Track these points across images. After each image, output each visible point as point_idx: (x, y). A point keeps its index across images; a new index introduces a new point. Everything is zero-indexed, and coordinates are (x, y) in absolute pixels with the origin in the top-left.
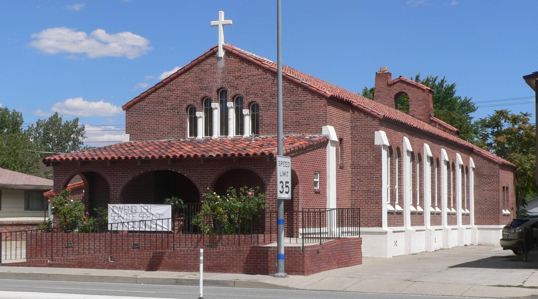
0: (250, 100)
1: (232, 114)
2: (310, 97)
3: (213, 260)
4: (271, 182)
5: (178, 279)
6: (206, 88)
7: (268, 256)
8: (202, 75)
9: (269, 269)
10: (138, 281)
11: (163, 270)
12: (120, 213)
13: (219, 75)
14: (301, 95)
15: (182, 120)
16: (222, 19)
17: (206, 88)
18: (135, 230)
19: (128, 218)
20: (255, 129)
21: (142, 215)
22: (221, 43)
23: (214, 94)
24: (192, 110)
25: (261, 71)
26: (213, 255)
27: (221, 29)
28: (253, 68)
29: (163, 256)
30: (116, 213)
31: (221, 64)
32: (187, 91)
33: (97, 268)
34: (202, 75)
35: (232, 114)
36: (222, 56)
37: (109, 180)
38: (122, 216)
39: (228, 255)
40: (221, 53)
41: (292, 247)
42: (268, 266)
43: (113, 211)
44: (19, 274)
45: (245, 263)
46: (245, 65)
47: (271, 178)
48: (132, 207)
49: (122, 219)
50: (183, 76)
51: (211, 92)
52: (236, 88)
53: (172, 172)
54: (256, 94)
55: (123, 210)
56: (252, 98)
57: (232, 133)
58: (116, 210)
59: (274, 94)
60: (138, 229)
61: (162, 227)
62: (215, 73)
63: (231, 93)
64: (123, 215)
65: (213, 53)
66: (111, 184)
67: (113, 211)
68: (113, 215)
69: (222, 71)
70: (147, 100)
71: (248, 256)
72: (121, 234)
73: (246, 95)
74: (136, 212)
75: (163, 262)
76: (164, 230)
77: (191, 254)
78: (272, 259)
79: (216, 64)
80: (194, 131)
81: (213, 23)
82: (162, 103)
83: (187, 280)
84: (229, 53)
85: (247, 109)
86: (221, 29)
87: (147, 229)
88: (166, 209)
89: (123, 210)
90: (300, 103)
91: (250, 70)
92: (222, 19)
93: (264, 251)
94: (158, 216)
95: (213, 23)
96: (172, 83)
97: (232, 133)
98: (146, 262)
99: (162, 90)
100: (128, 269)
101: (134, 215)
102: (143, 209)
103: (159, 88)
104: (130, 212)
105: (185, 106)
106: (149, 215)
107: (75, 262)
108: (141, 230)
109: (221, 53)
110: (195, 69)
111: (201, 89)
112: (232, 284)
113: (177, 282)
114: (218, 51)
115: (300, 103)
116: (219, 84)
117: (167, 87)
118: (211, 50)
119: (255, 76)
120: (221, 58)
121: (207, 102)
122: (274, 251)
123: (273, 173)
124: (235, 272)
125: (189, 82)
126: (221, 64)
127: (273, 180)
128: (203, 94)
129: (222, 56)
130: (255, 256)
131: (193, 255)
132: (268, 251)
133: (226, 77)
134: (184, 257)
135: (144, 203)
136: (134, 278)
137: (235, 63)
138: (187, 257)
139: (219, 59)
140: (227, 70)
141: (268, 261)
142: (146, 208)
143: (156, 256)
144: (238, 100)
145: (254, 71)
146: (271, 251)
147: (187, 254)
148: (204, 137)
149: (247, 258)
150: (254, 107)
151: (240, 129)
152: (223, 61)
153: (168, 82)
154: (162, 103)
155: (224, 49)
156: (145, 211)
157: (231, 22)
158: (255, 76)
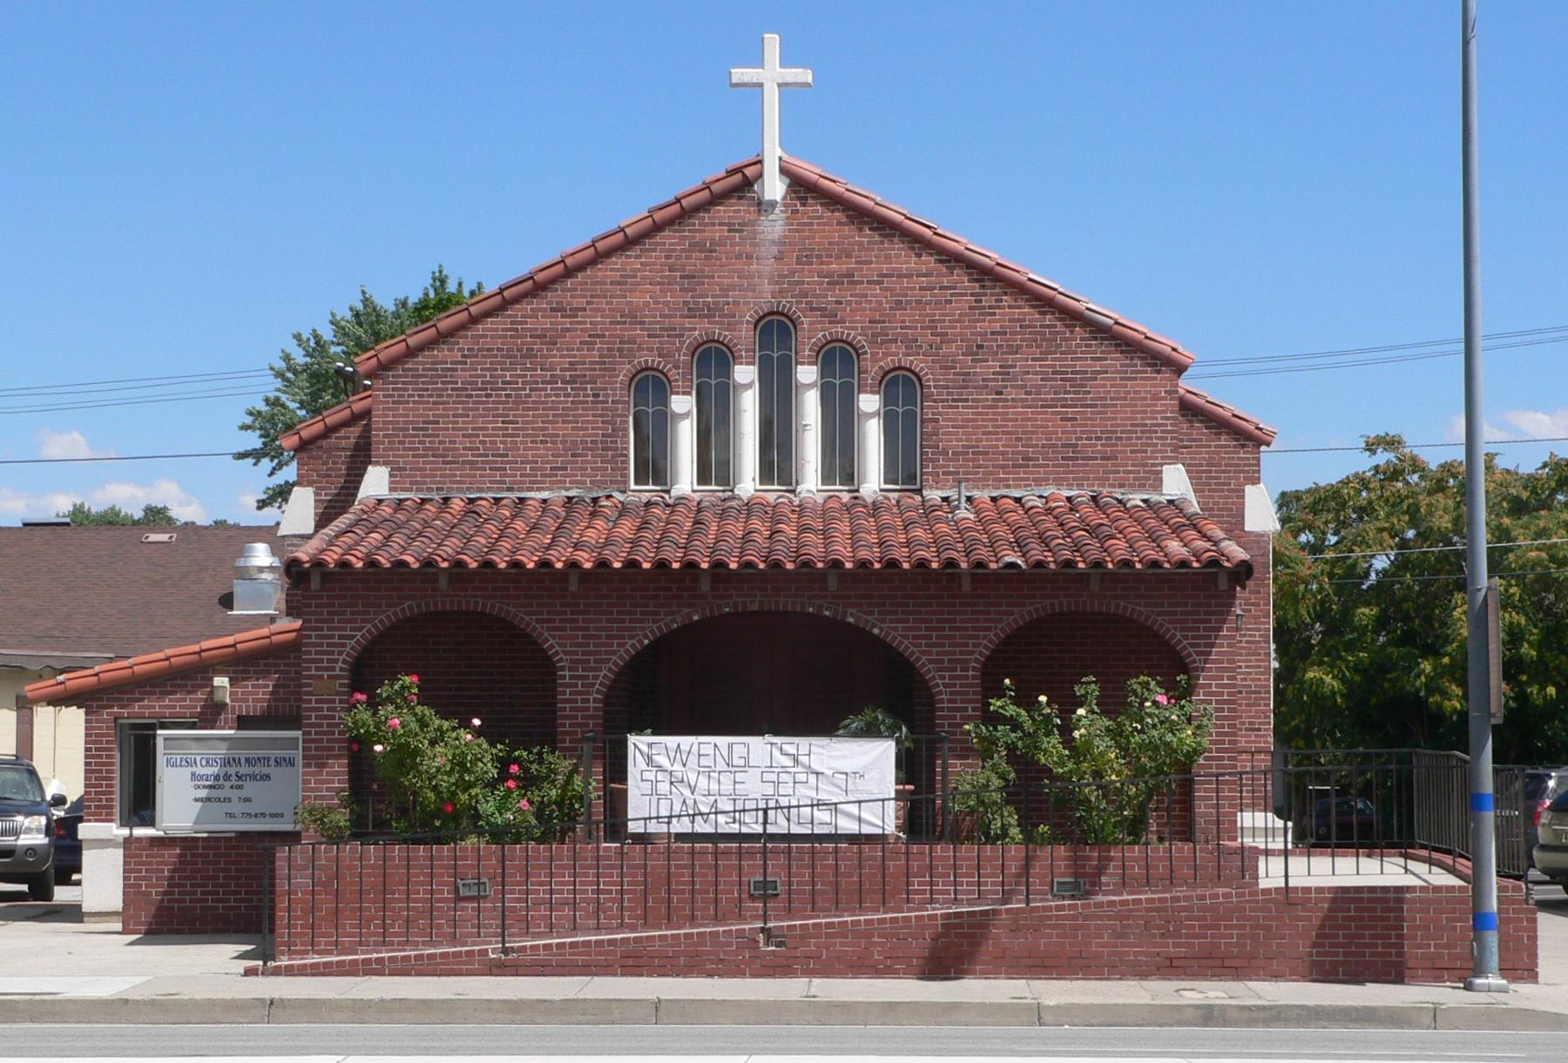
0: (889, 362)
1: (811, 407)
2: (1115, 361)
3: (1188, 936)
4: (1214, 662)
5: (1210, 1007)
6: (711, 312)
7: (1402, 919)
8: (695, 262)
9: (1410, 963)
10: (1046, 1018)
11: (985, 974)
12: (677, 767)
13: (768, 266)
14: (1085, 356)
15: (613, 423)
16: (772, 72)
17: (711, 312)
18: (745, 830)
19: (714, 787)
20: (904, 466)
21: (774, 777)
22: (773, 154)
23: (744, 335)
24: (651, 387)
25: (929, 261)
26: (1187, 919)
27: (772, 97)
28: (897, 248)
29: (986, 926)
30: (660, 768)
31: (774, 226)
32: (633, 317)
33: (711, 975)
34: (695, 262)
35: (811, 407)
36: (778, 199)
37: (553, 645)
38: (685, 780)
39: (1248, 918)
40: (774, 188)
41: (1385, 889)
42: (1402, 954)
43: (649, 760)
44: (522, 1002)
45: (1314, 945)
46: (867, 236)
47: (1212, 645)
48: (730, 746)
49: (687, 792)
50: (617, 261)
51: (731, 326)
52: (832, 317)
53: (818, 617)
54: (911, 344)
55: (693, 759)
56: (896, 356)
57: (811, 481)
58: (662, 760)
59: (980, 347)
60: (759, 829)
61: (860, 819)
62: (749, 257)
63: (811, 332)
64: (692, 777)
65: (742, 184)
66: (562, 660)
67: (649, 760)
68: (647, 775)
69: (774, 250)
70: (463, 343)
71: (1325, 918)
72: (662, 845)
73: (872, 343)
74: (747, 765)
75: (989, 946)
76: (866, 830)
77: (1101, 918)
78: (1416, 928)
79: (753, 223)
80: (654, 467)
81: (740, 74)
82: (530, 354)
83: (1249, 1008)
84: (801, 187)
85: (872, 392)
86: (772, 97)
87: (796, 830)
88: (868, 758)
89: (693, 759)
90: (1078, 382)
91: (887, 257)
92: (772, 72)
93: (1386, 900)
94: (847, 779)
95: (740, 74)
96: (569, 283)
97: (811, 481)
98: (919, 948)
99: (527, 306)
100: (841, 974)
101: (739, 777)
102: (776, 753)
103: (516, 300)
104: (721, 766)
105: (624, 371)
106: (802, 777)
107: (614, 953)
108: (771, 829)
109: (774, 188)
110: (667, 237)
111: (692, 312)
112: (1428, 1020)
113: (1209, 1015)
114: (760, 175)
115: (1078, 382)
116: (765, 296)
117: (552, 298)
118: (731, 173)
119: (909, 276)
120: (773, 204)
121: (712, 362)
122: (1421, 901)
123: (1220, 629)
124: (1276, 976)
125: (643, 284)
126: (774, 226)
127: (1218, 653)
128: (699, 329)
129: (778, 199)
130: (1353, 919)
131: (1110, 918)
132: (1401, 901)
133: (792, 273)
134: (1072, 927)
135: (777, 733)
136: (1029, 1008)
137: (829, 227)
138: (1086, 927)
139: (762, 206)
140: (798, 252)
141: (1401, 937)
142: (791, 749)
143: (960, 926)
144: (839, 363)
145: (903, 259)
146: (1413, 901)
147: (1086, 918)
148: (696, 487)
149: (1322, 927)
150: (901, 388)
151: (841, 459)
152: (778, 214)
153: (554, 280)
154: (530, 354)
155: (784, 171)
156: (788, 762)
157: (806, 76)
158: (909, 276)
